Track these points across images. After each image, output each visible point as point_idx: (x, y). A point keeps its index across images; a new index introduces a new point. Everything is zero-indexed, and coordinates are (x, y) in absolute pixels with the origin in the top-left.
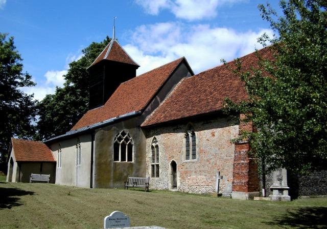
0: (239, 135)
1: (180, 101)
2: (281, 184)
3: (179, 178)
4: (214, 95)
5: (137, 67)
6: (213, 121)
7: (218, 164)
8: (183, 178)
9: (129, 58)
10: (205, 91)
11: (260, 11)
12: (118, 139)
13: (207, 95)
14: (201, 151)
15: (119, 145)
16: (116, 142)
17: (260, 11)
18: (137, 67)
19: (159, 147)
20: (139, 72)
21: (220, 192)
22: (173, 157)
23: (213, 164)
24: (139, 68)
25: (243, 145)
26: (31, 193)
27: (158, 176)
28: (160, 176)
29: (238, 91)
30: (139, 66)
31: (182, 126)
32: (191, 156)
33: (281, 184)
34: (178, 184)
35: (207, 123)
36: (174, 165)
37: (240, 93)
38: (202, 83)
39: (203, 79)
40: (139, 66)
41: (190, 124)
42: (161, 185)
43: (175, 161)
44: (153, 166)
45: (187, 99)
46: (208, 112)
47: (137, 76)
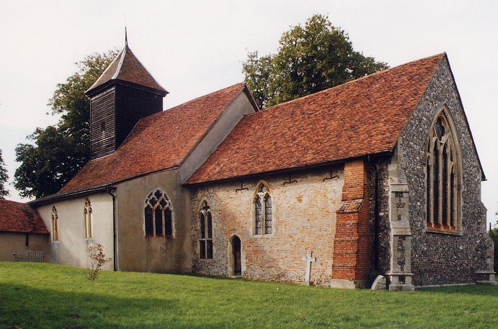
0: (343, 200)
1: (243, 149)
2: (402, 269)
3: (245, 261)
4: (300, 141)
5: (164, 93)
6: (300, 180)
7: (306, 240)
8: (250, 260)
9: (149, 76)
10: (283, 135)
11: (68, 80)
12: (150, 202)
13: (287, 142)
14: (280, 223)
15: (161, 211)
16: (148, 206)
17: (68, 80)
18: (164, 93)
19: (213, 215)
20: (168, 104)
21: (312, 280)
22: (235, 230)
23: (299, 241)
24: (167, 95)
25: (349, 215)
26: (490, 223)
27: (210, 256)
28: (214, 257)
29: (339, 136)
30: (168, 93)
31: (250, 185)
32: (260, 231)
33: (402, 269)
34: (244, 268)
35: (290, 182)
36: (236, 242)
37: (343, 140)
38: (275, 123)
39: (277, 117)
40: (168, 93)
41: (261, 183)
42: (216, 270)
43: (238, 236)
44: (202, 243)
45: (254, 147)
46: (293, 166)
47: (164, 109)
